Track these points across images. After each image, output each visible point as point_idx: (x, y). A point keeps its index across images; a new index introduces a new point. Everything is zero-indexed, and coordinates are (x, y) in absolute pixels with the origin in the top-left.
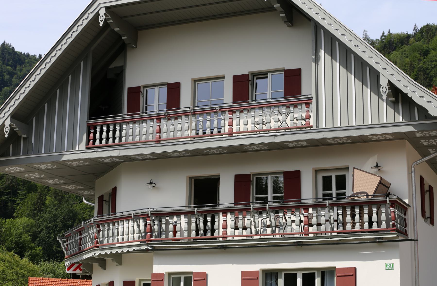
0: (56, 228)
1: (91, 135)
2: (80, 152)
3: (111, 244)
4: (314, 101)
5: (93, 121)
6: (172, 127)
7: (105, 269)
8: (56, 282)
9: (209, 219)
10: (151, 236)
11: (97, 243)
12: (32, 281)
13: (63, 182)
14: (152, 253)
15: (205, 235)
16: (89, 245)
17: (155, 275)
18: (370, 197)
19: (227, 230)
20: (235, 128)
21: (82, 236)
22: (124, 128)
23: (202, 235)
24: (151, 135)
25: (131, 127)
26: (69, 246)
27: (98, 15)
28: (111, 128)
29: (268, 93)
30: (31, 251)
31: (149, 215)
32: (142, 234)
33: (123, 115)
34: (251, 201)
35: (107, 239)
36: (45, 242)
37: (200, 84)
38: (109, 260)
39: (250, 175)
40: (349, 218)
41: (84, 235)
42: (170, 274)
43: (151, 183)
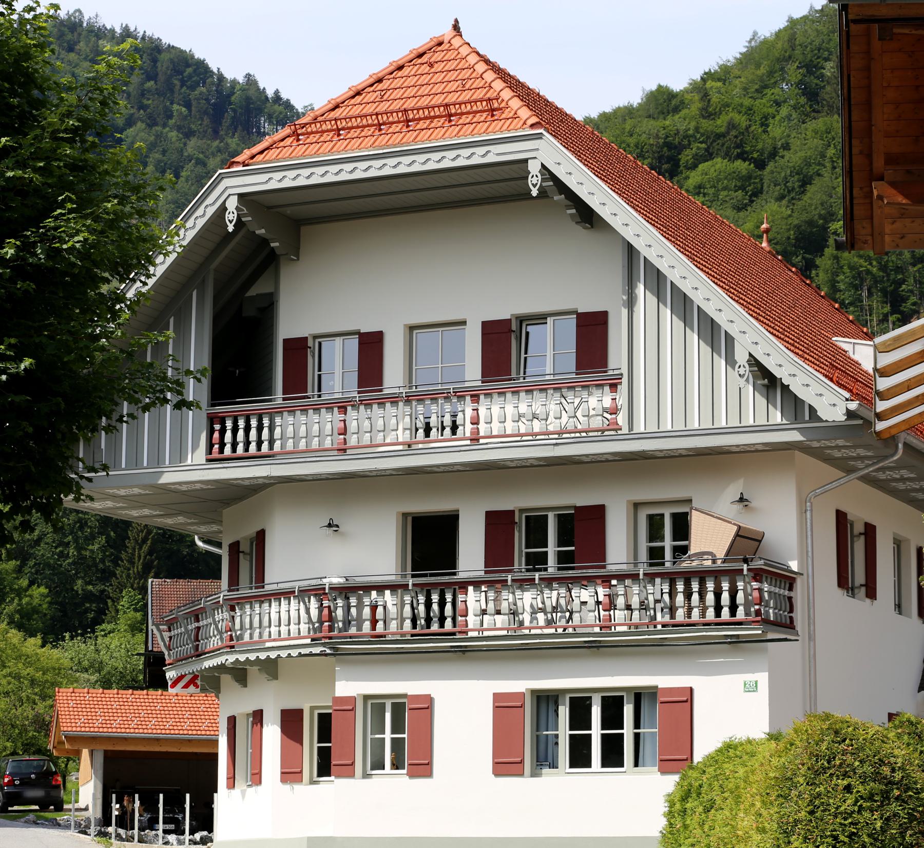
0: (81, 528)
1: (216, 435)
2: (194, 468)
3: (256, 642)
4: (625, 380)
5: (219, 409)
6: (367, 423)
7: (245, 686)
8: (121, 700)
9: (435, 598)
10: (331, 629)
11: (231, 639)
12: (65, 698)
13: (158, 513)
14: (332, 659)
15: (428, 627)
16: (214, 642)
17: (338, 700)
18: (719, 562)
19: (467, 618)
20: (483, 428)
21: (201, 623)
22: (277, 424)
23: (422, 628)
24: (329, 438)
25: (290, 423)
26: (174, 640)
27: (223, 209)
28: (254, 423)
29: (548, 354)
30: (20, 600)
31: (327, 591)
32: (313, 625)
33: (274, 400)
34: (516, 566)
35: (249, 631)
36: (52, 570)
37: (418, 351)
38: (253, 671)
39: (513, 511)
40: (680, 599)
41: (205, 622)
42: (366, 698)
43: (330, 525)
